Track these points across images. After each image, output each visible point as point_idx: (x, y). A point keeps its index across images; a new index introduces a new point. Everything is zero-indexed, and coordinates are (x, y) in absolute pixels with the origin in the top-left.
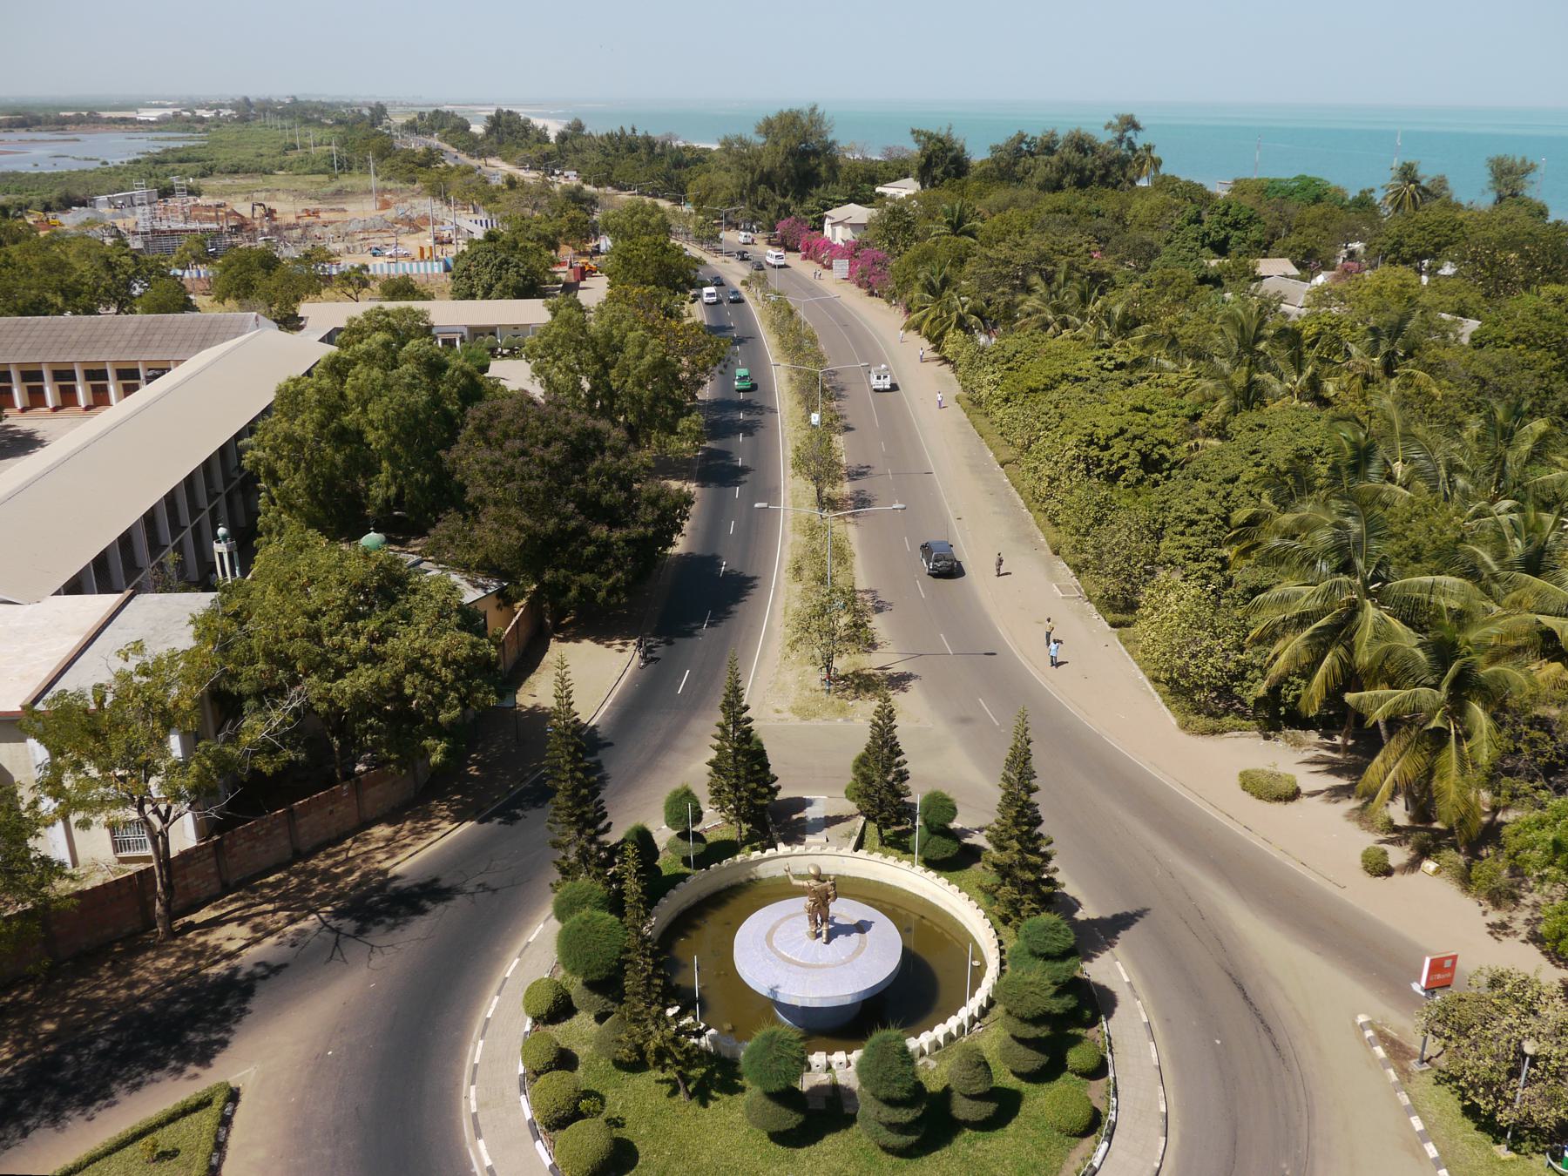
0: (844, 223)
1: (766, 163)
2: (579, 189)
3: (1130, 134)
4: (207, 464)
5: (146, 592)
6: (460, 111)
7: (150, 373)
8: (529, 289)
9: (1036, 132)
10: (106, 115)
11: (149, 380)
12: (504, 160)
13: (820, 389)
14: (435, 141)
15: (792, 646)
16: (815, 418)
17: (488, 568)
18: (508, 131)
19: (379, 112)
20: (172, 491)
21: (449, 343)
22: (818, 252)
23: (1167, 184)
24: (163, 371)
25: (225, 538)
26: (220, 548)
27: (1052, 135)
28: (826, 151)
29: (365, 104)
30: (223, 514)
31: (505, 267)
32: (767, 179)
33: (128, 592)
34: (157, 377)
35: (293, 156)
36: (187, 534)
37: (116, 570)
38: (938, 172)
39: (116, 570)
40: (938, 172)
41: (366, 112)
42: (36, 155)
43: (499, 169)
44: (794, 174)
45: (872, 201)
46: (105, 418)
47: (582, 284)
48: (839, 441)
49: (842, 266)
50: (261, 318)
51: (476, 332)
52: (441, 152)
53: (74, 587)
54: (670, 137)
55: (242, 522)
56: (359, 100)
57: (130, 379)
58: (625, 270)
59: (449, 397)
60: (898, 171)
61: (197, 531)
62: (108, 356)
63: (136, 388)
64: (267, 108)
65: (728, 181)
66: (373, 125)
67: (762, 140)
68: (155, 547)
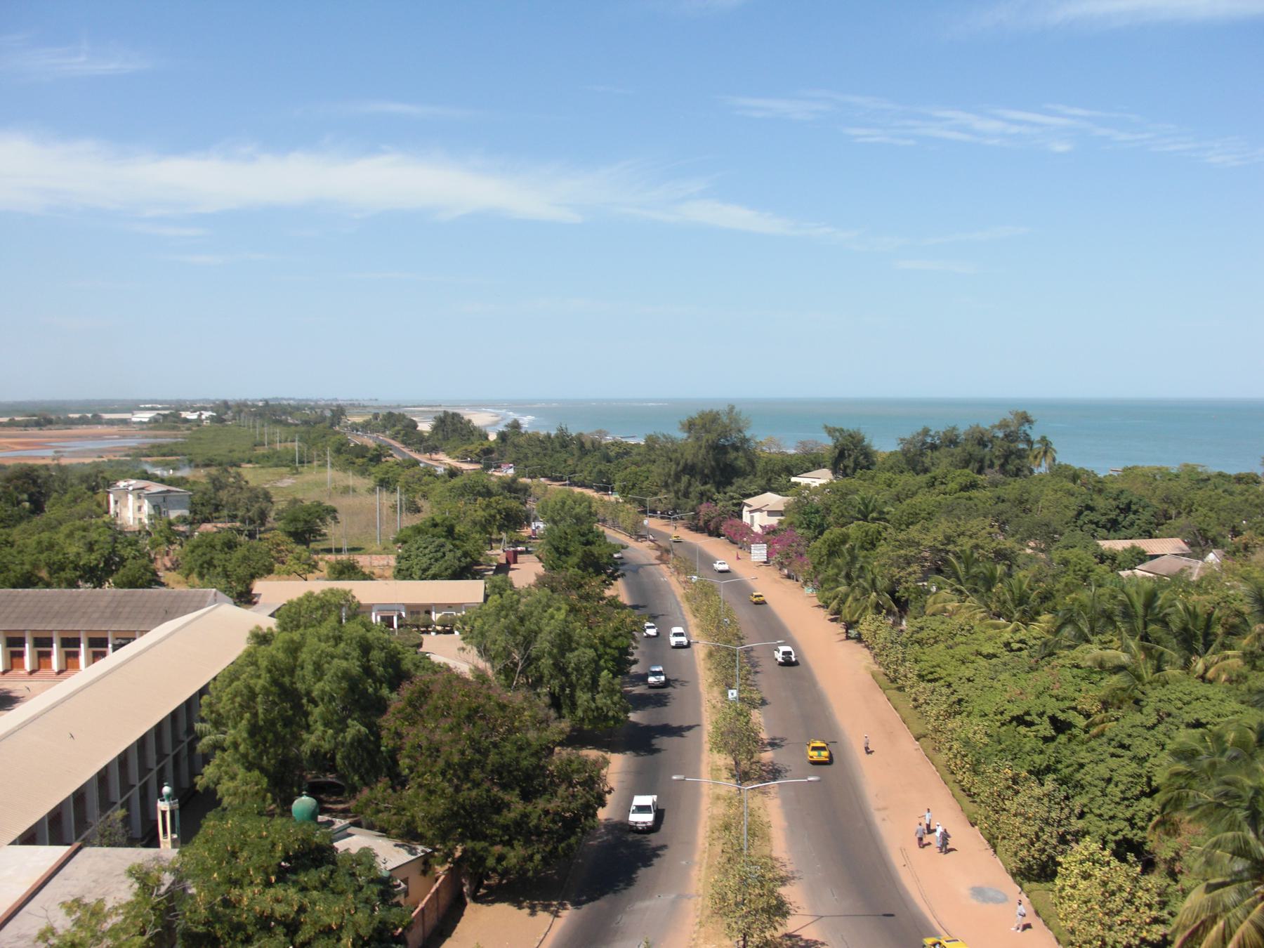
0: (762, 511)
1: (689, 457)
2: (514, 480)
3: (1026, 427)
4: (159, 727)
5: (93, 845)
6: (407, 411)
7: (117, 642)
8: (461, 573)
9: (938, 427)
10: (107, 416)
11: (115, 648)
12: (448, 454)
13: (734, 662)
14: (385, 438)
15: (701, 924)
16: (733, 694)
17: (408, 836)
18: (452, 429)
19: (339, 412)
20: (106, 767)
21: (388, 621)
22: (741, 538)
23: (1061, 472)
24: (129, 640)
25: (169, 796)
26: (163, 806)
27: (954, 429)
28: (741, 446)
29: (327, 406)
30: (169, 772)
31: (447, 550)
32: (690, 469)
33: (77, 844)
34: (123, 645)
35: (261, 451)
36: (135, 793)
37: (63, 826)
38: (850, 462)
39: (63, 826)
40: (850, 462)
41: (328, 413)
42: (39, 452)
43: (443, 461)
44: (712, 467)
45: (787, 489)
46: (102, 665)
47: (513, 566)
48: (757, 716)
49: (759, 552)
50: (220, 594)
51: (413, 610)
52: (391, 447)
53: (29, 838)
54: (602, 433)
55: (185, 784)
56: (322, 403)
57: (99, 646)
58: (558, 552)
59: (382, 671)
60: (815, 463)
61: (144, 789)
62: (82, 627)
63: (104, 655)
64: (241, 408)
65: (657, 471)
66: (332, 425)
67: (685, 435)
68: (106, 804)
